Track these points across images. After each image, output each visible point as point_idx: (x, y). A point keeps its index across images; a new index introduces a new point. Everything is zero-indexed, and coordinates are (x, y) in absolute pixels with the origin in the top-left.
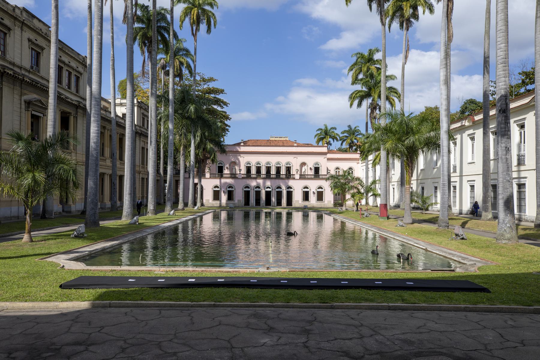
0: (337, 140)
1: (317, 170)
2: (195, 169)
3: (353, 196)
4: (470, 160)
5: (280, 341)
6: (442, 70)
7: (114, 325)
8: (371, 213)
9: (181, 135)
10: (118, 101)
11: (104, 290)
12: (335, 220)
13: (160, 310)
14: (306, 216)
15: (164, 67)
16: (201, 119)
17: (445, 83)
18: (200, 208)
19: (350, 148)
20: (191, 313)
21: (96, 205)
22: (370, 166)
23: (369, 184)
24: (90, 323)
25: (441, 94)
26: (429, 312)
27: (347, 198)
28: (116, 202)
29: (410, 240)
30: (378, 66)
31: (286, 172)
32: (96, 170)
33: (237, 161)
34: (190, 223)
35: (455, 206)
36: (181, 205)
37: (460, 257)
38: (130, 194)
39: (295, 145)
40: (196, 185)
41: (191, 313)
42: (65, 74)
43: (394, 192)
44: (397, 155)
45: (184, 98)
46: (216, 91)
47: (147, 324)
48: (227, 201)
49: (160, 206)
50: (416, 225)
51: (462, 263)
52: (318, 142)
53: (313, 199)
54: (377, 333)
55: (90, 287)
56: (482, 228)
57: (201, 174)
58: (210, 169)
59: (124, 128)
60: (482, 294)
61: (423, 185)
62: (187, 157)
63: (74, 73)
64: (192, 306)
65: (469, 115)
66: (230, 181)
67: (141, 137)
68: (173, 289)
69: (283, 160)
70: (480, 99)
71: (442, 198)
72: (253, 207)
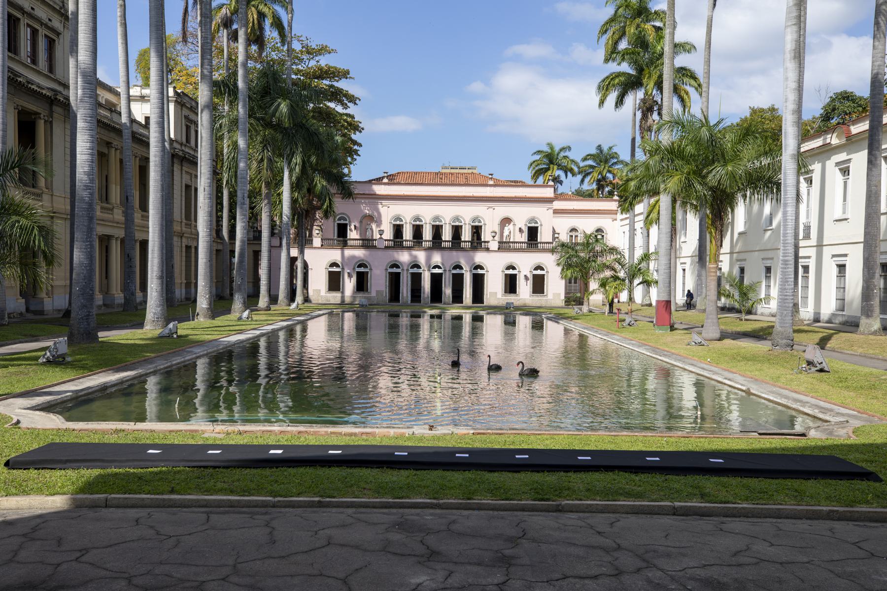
0: (574, 175)
1: (533, 233)
2: (292, 231)
3: (603, 285)
4: (839, 215)
5: (450, 581)
6: (789, 30)
7: (111, 546)
8: (639, 318)
9: (262, 160)
10: (135, 91)
11: (96, 472)
12: (567, 331)
13: (207, 513)
14: (510, 323)
15: (227, 23)
16: (301, 131)
17: (795, 57)
18: (301, 307)
19: (598, 189)
20: (272, 519)
21: (91, 298)
22: (639, 225)
23: (636, 261)
24: (59, 541)
25: (786, 79)
26: (755, 520)
27: (591, 289)
28: (133, 294)
29: (715, 373)
30: (658, 24)
31: (473, 236)
32: (90, 230)
33: (376, 214)
34: (282, 335)
35: (806, 305)
36: (263, 301)
37: (817, 407)
38: (161, 277)
39: (491, 182)
40: (293, 260)
41: (272, 519)
42: (24, 34)
43: (684, 277)
44: (692, 204)
45: (269, 86)
46: (333, 73)
47: (179, 542)
48: (354, 293)
49: (221, 303)
50: (728, 342)
51: (820, 419)
52: (536, 176)
53: (524, 289)
54: (650, 565)
55: (68, 465)
56: (860, 350)
57: (304, 241)
58: (322, 230)
59: (147, 145)
60: (863, 485)
61: (743, 264)
62: (274, 204)
63: (42, 32)
64: (274, 505)
65: (839, 123)
66: (360, 253)
67: (184, 164)
68: (238, 470)
69: (467, 214)
70: (863, 90)
71: (782, 290)
72: (405, 305)
